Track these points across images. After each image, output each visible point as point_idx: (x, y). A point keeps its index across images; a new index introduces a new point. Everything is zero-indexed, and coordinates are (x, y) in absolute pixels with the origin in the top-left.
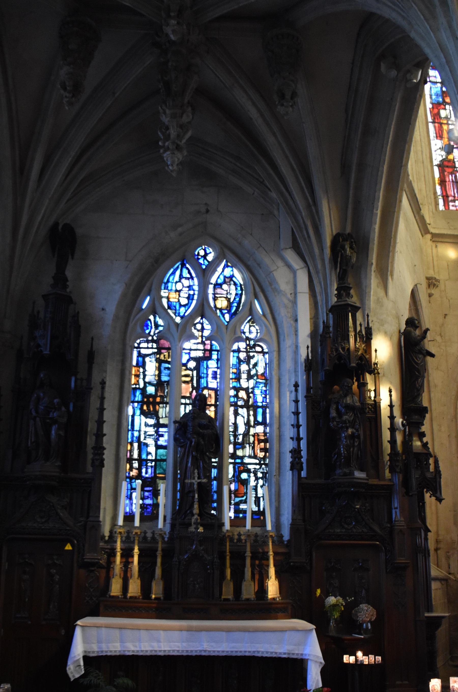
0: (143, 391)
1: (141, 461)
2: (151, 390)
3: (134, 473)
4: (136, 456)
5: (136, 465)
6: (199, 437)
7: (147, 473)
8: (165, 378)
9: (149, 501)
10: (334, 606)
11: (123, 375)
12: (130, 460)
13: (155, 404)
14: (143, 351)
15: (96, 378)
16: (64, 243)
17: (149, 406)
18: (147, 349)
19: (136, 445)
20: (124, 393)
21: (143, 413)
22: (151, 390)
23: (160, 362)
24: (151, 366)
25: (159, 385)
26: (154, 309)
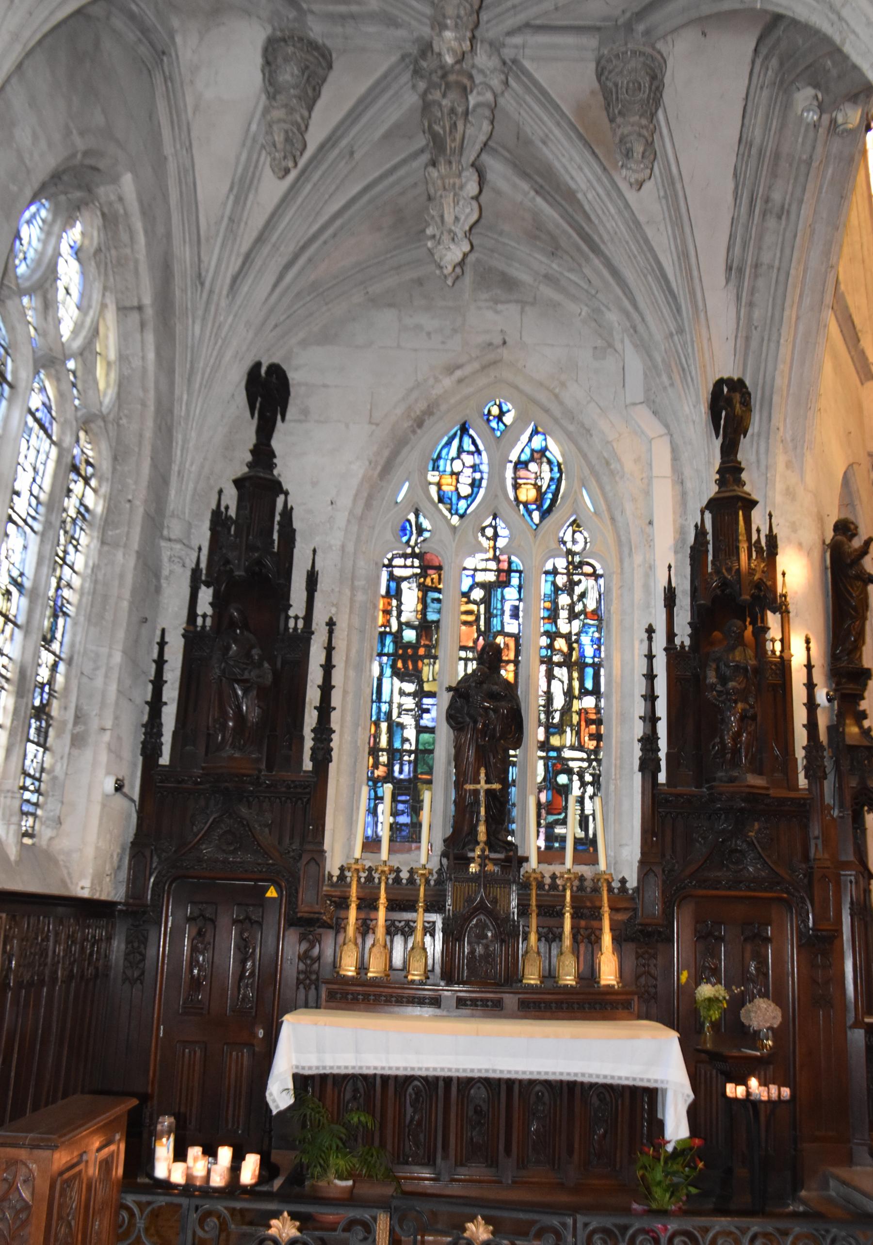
0: (397, 637)
1: (394, 754)
2: (410, 635)
3: (381, 772)
4: (384, 743)
5: (384, 758)
8: (432, 616)
9: (404, 819)
10: (711, 1001)
13: (416, 658)
14: (398, 572)
21: (396, 673)
22: (410, 635)
23: (424, 589)
25: (425, 627)
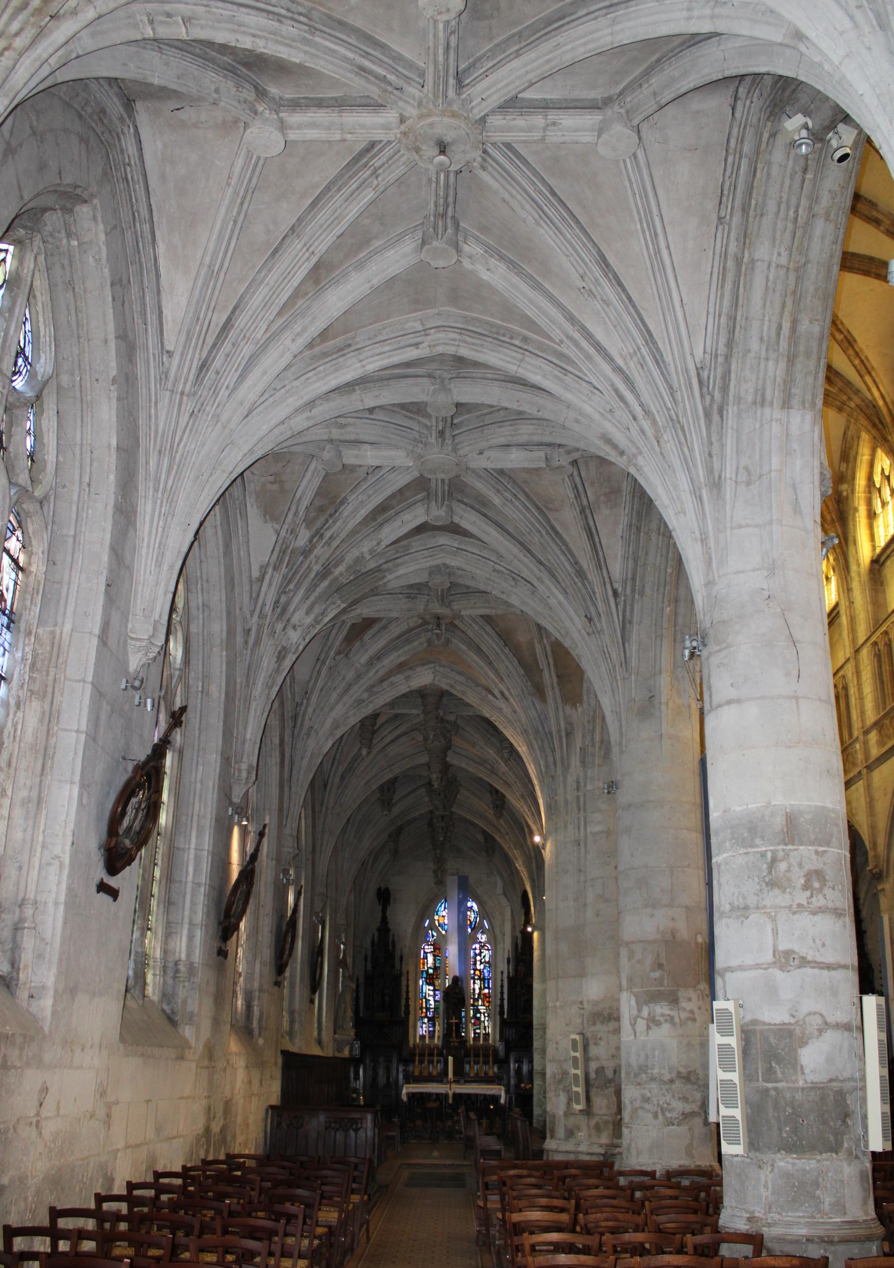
1: (428, 1009)
2: (431, 971)
6: (455, 997)
7: (430, 1015)
11: (417, 966)
12: (421, 1008)
15: (404, 970)
16: (384, 896)
17: (430, 980)
18: (429, 949)
19: (431, 22)
20: (418, 974)
22: (431, 971)
23: (434, 956)
24: (430, 958)
25: (435, 968)
26: (432, 927)
